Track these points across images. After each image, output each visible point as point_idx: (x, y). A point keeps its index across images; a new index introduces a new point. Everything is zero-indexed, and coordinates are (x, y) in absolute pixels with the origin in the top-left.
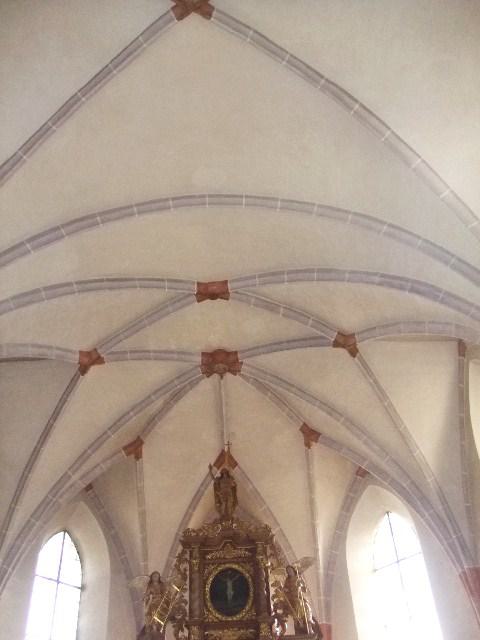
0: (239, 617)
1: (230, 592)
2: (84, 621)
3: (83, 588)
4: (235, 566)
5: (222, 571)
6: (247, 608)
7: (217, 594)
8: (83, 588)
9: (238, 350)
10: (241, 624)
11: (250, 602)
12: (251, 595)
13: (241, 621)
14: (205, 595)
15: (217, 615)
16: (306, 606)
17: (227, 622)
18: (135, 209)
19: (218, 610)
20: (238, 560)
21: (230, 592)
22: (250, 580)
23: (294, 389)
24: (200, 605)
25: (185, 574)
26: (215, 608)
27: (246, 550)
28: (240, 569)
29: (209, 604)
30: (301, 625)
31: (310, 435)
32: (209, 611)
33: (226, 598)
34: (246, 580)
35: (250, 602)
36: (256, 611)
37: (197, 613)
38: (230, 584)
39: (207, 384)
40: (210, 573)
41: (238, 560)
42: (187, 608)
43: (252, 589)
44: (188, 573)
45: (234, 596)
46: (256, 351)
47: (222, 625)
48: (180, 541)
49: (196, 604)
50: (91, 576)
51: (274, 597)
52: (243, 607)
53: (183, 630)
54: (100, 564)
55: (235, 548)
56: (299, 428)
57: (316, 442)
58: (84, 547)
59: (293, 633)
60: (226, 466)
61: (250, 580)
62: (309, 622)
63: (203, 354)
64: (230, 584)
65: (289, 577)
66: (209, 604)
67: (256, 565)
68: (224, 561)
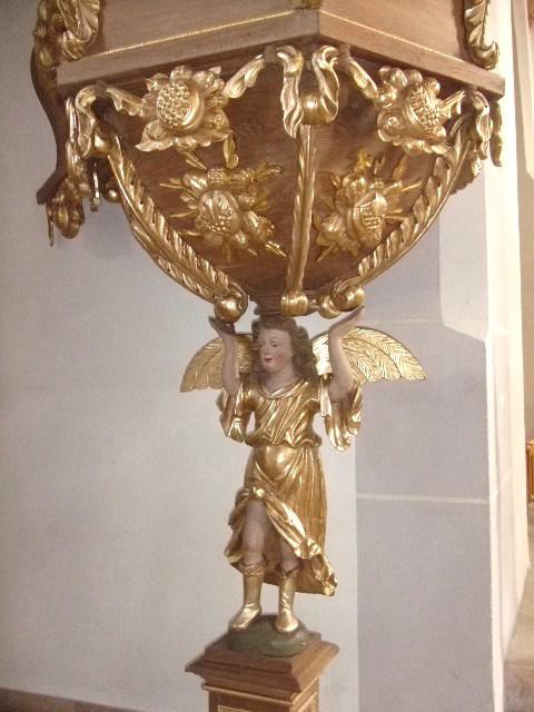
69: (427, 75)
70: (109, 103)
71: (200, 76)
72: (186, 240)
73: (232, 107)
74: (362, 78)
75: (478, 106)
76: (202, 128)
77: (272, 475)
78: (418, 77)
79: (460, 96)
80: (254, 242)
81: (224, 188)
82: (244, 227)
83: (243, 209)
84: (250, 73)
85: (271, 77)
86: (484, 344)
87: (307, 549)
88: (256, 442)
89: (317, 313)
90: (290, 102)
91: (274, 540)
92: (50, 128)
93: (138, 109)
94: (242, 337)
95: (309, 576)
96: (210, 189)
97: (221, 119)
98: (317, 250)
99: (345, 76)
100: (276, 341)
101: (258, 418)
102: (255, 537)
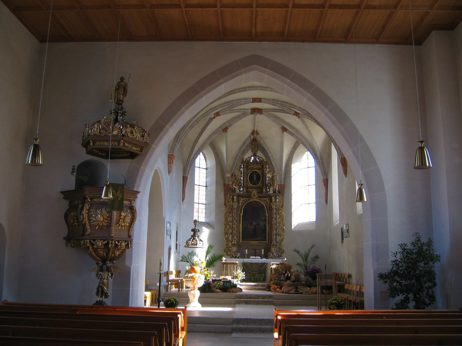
0: (256, 186)
1: (255, 178)
2: (208, 179)
3: (206, 169)
4: (256, 171)
5: (253, 172)
6: (260, 183)
7: (251, 178)
8: (206, 169)
9: (260, 134)
10: (257, 188)
11: (261, 182)
12: (261, 179)
13: (258, 187)
14: (247, 179)
15: (251, 185)
16: (277, 185)
17: (254, 187)
18: (237, 91)
19: (251, 183)
20: (257, 169)
21: (255, 178)
22: (261, 175)
23: (280, 120)
24: (246, 182)
25: (242, 172)
26: (250, 183)
27: (260, 166)
28: (258, 172)
29: (249, 181)
30: (275, 190)
31: (284, 129)
32: (248, 183)
33: (254, 179)
34: (260, 175)
35: (261, 182)
36: (262, 184)
37: (245, 184)
38: (255, 176)
39: (251, 116)
40: (249, 172)
41: (257, 169)
42: (242, 182)
43: (261, 178)
44: (242, 172)
45: (256, 180)
46: (268, 110)
47: (252, 188)
48: (241, 162)
49: (245, 182)
50: (209, 166)
51: (268, 180)
52: (259, 182)
53: (241, 188)
54: (212, 162)
55: (257, 165)
56: (280, 128)
57: (286, 132)
58: (206, 156)
59: (272, 193)
60: (255, 135)
61: (261, 175)
62: (277, 190)
63: (251, 109)
64: (255, 176)
65: (272, 177)
66: (249, 181)
67: (263, 171)
68: (253, 169)
69: (123, 241)
70: (91, 241)
71: (101, 241)
72: (96, 255)
73: (104, 244)
74: (117, 243)
75: (129, 242)
76: (101, 246)
77: (103, 283)
78: (122, 241)
79: (127, 242)
80: (104, 256)
81: (102, 251)
82: (103, 255)
83: (103, 253)
84: (106, 242)
85: (108, 243)
86: (130, 268)
87: (106, 291)
88: (101, 279)
89: (73, 188)
90: (110, 245)
91: (103, 290)
92: (67, 229)
93: (94, 243)
94: (100, 266)
95: (106, 296)
96: (100, 251)
97: (103, 246)
98: (111, 257)
99: (115, 242)
100: (105, 267)
101: (101, 276)
102: (100, 290)
